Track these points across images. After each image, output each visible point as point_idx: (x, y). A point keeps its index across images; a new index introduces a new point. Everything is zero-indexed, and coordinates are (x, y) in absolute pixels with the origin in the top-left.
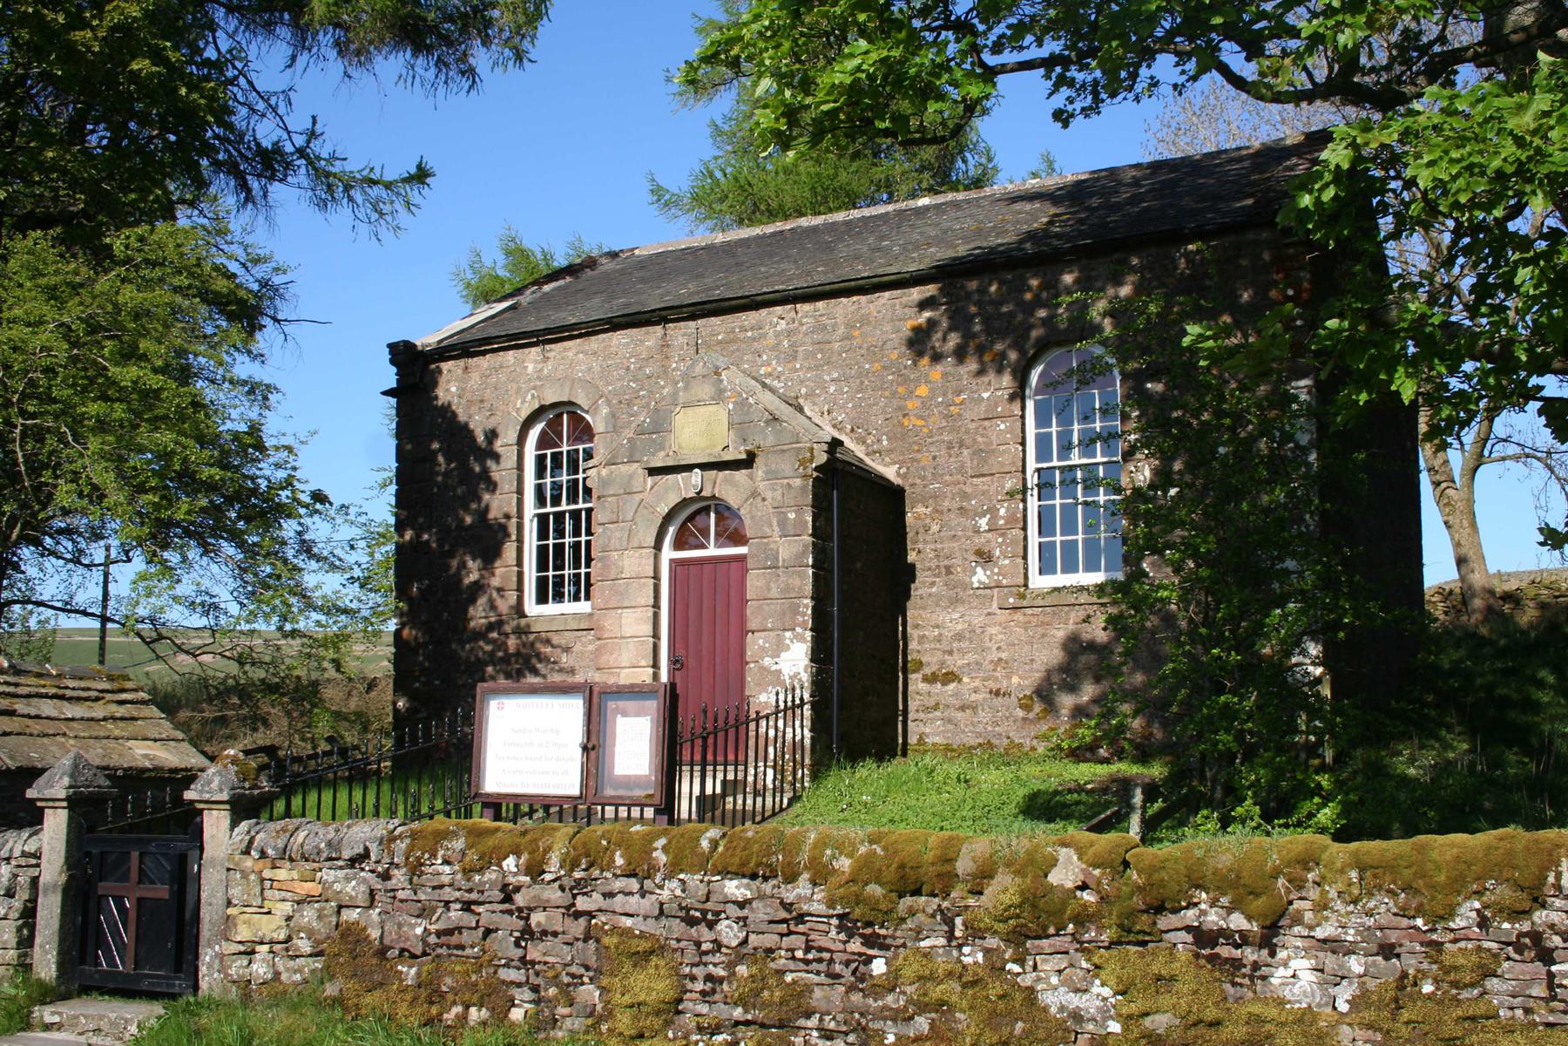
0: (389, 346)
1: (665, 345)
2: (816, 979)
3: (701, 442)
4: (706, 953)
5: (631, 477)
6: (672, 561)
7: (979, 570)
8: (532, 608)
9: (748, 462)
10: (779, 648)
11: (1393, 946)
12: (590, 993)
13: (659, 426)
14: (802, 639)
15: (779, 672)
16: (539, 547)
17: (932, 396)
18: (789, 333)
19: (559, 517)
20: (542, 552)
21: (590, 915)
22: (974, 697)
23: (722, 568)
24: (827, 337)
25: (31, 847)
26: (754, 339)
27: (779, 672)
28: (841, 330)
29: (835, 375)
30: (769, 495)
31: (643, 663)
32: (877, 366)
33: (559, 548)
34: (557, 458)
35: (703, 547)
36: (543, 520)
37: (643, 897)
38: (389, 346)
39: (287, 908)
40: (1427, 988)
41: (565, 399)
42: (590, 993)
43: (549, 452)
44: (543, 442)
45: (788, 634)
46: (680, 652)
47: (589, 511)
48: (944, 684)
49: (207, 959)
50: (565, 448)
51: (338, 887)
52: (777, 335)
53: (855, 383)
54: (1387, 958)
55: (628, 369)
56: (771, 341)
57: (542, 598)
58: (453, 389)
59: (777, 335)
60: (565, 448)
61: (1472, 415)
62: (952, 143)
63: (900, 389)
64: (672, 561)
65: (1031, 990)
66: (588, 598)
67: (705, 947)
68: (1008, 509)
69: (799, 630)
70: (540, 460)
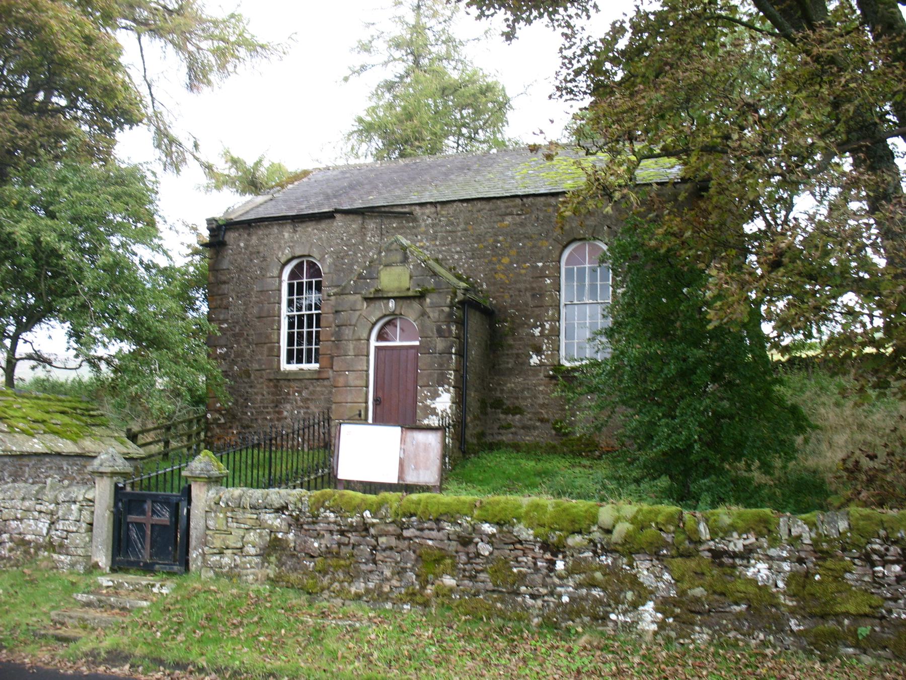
0: (207, 220)
1: (363, 227)
2: (529, 571)
3: (396, 284)
4: (471, 558)
5: (355, 302)
6: (376, 347)
7: (534, 356)
8: (285, 366)
9: (421, 296)
10: (435, 395)
11: (803, 559)
12: (411, 576)
13: (373, 276)
14: (448, 391)
15: (435, 408)
16: (289, 333)
17: (511, 263)
18: (433, 225)
19: (300, 317)
20: (290, 336)
21: (410, 539)
22: (530, 422)
23: (404, 352)
24: (454, 229)
25: (90, 496)
26: (414, 227)
27: (435, 408)
28: (462, 226)
29: (458, 249)
30: (431, 315)
31: (360, 400)
32: (481, 245)
33: (300, 335)
34: (300, 285)
35: (393, 340)
36: (291, 318)
37: (439, 531)
38: (207, 220)
39: (242, 533)
40: (817, 577)
41: (306, 253)
42: (411, 576)
43: (295, 282)
44: (293, 275)
45: (441, 389)
46: (380, 395)
47: (318, 315)
48: (514, 415)
49: (194, 556)
50: (305, 280)
51: (270, 522)
52: (427, 226)
53: (469, 254)
54: (801, 564)
55: (342, 239)
56: (423, 229)
57: (289, 362)
58: (242, 245)
59: (427, 226)
60: (305, 280)
61: (658, 195)
62: (499, 114)
63: (494, 259)
64: (376, 347)
65: (635, 575)
66: (316, 362)
67: (471, 555)
68: (551, 325)
69: (446, 387)
70: (291, 287)
